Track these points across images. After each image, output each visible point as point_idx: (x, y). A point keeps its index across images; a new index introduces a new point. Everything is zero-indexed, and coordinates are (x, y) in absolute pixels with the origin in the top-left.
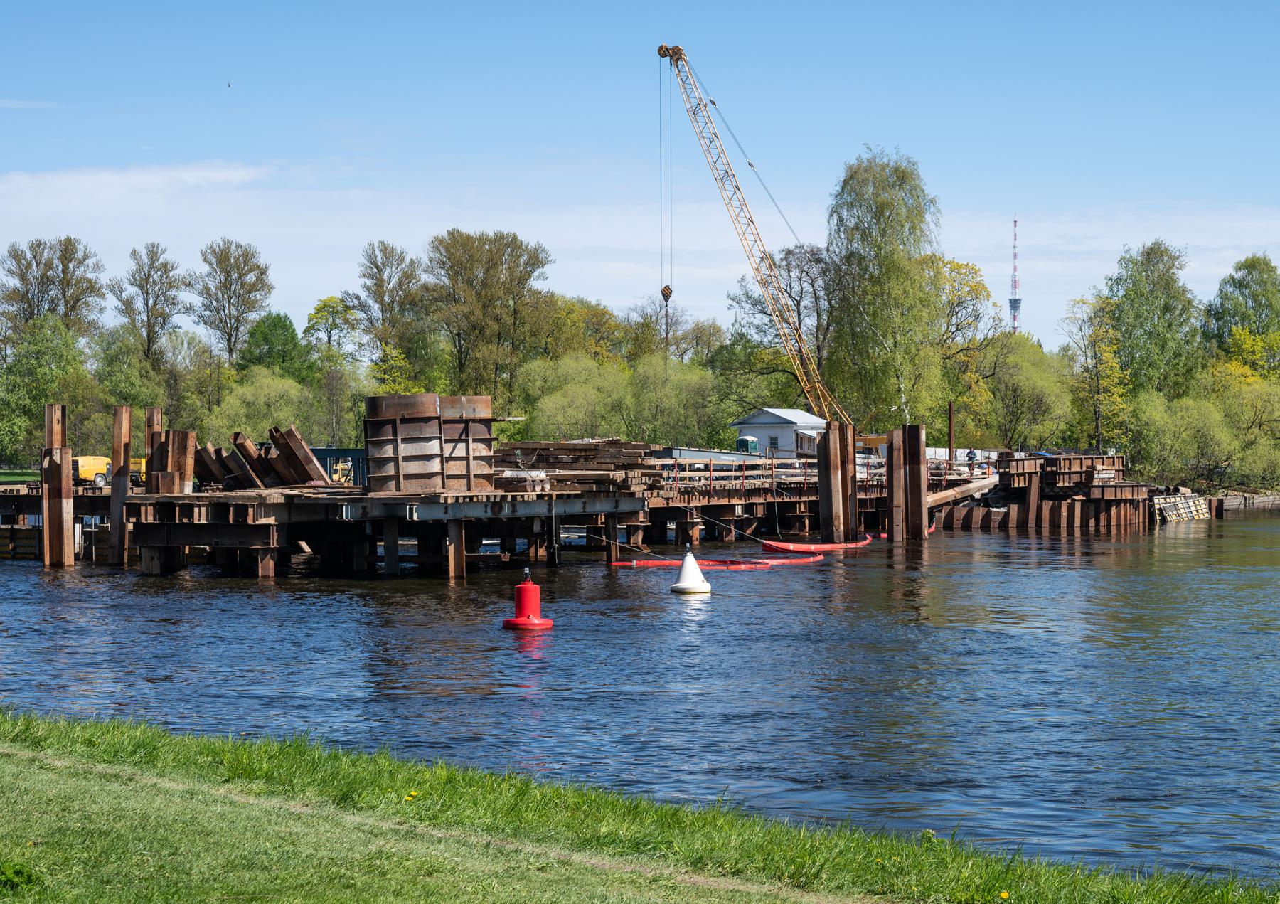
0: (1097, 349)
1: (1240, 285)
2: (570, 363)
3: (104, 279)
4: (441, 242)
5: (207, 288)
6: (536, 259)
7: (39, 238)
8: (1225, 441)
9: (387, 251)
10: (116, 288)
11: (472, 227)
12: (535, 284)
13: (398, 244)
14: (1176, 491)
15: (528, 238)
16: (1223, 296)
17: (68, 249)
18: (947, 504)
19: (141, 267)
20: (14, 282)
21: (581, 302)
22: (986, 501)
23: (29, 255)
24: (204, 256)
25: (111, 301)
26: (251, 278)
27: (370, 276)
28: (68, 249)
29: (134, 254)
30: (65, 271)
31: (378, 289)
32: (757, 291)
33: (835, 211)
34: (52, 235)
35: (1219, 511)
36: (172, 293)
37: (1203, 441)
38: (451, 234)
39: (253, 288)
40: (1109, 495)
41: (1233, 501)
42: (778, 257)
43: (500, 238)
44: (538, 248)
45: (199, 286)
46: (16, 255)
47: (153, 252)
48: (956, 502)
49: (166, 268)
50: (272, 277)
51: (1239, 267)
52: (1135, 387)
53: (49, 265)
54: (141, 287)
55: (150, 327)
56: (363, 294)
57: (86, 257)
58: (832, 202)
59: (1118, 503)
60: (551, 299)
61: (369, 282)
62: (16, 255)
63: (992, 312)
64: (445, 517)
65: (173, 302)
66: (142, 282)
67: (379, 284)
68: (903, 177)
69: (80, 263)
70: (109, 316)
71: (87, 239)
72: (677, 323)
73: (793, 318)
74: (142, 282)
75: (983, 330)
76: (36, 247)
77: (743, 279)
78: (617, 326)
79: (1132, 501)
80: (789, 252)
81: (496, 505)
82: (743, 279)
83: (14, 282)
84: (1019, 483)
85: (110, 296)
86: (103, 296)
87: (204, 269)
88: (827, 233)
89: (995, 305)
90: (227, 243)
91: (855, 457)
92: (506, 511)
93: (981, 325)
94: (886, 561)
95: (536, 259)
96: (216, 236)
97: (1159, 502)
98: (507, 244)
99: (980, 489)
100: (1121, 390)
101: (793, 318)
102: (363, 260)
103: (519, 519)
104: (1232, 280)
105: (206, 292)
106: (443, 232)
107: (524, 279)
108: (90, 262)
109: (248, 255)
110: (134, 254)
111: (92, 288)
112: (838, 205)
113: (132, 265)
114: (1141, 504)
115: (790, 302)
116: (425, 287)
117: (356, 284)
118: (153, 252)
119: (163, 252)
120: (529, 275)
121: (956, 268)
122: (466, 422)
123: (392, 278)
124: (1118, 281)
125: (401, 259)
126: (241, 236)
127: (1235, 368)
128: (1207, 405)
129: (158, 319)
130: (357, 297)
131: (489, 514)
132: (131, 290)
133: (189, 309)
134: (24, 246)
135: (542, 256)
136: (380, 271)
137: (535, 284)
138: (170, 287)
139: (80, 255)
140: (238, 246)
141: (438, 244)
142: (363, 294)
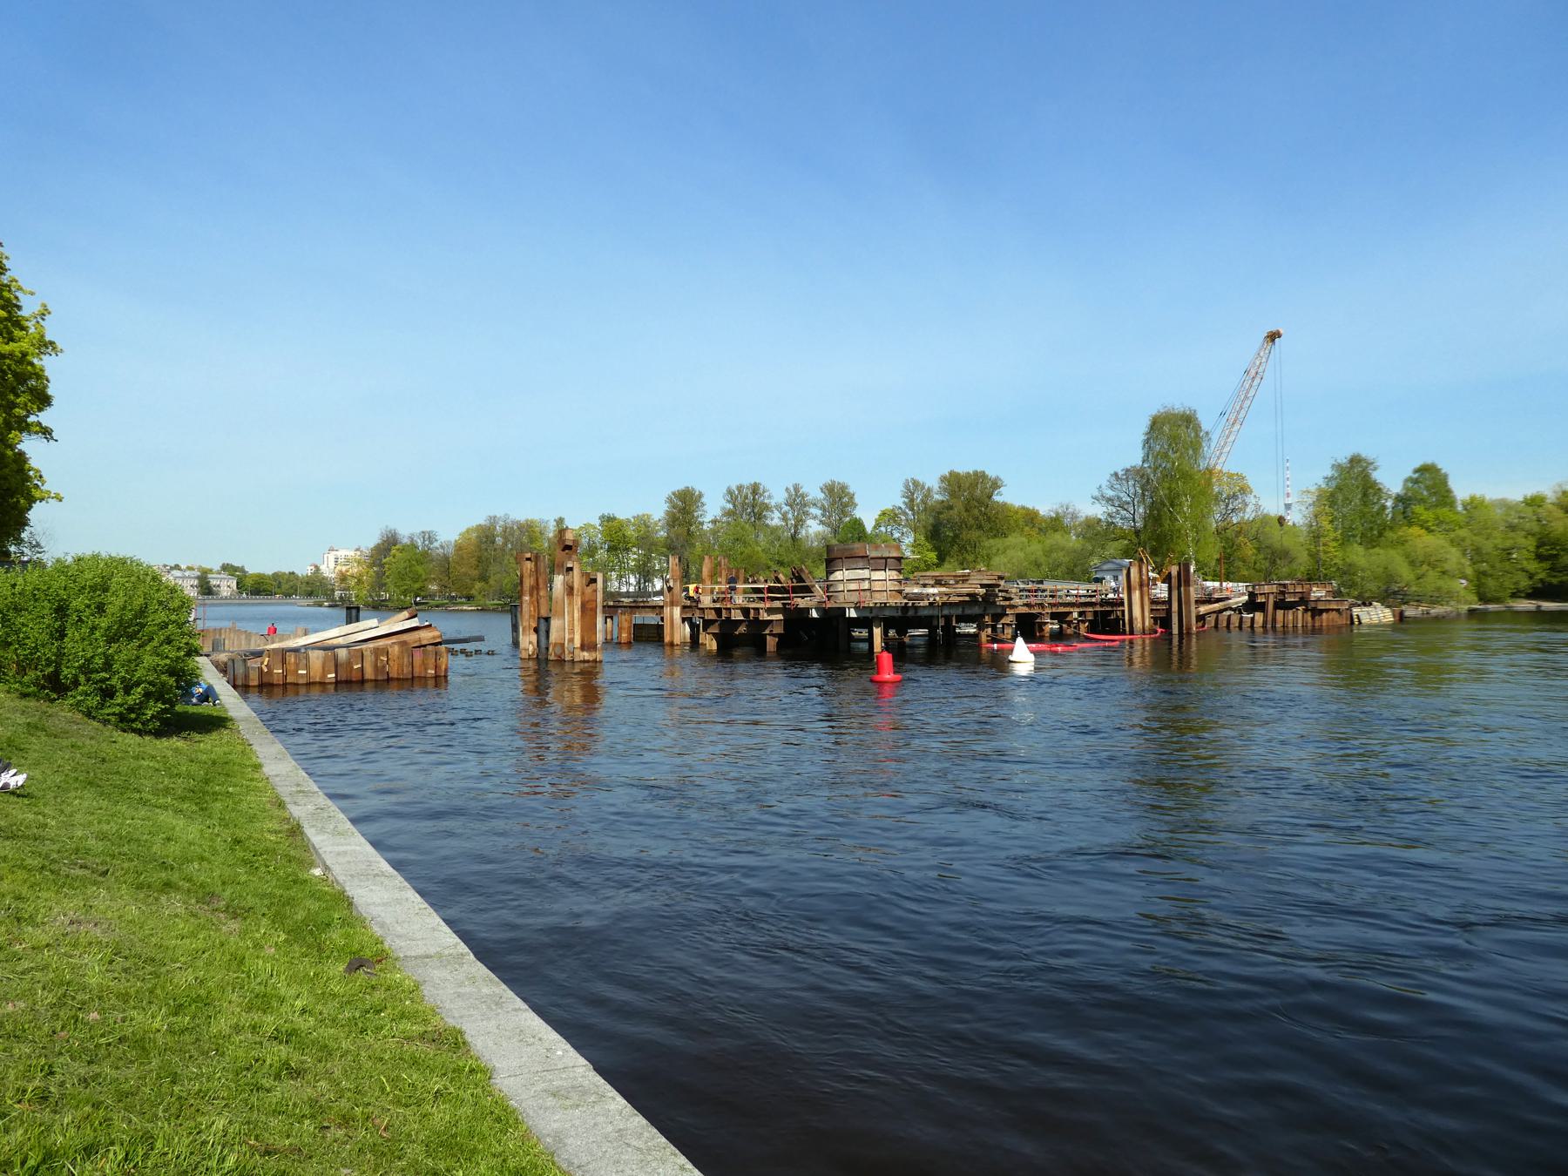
1: (1416, 481)
2: (1013, 539)
5: (823, 505)
6: (996, 484)
8: (1405, 573)
9: (916, 483)
10: (779, 507)
12: (996, 498)
13: (921, 479)
14: (1370, 604)
15: (991, 473)
16: (1405, 488)
17: (755, 489)
18: (1214, 612)
19: (790, 495)
20: (730, 506)
21: (1023, 508)
22: (1238, 610)
25: (777, 515)
26: (846, 499)
27: (907, 497)
28: (755, 489)
29: (787, 489)
30: (754, 499)
31: (911, 503)
32: (1110, 493)
33: (1147, 441)
34: (747, 481)
35: (1401, 617)
36: (807, 509)
37: (1390, 578)
38: (951, 473)
39: (847, 505)
40: (1321, 606)
41: (1410, 612)
42: (1120, 473)
43: (976, 473)
44: (998, 478)
45: (819, 505)
46: (730, 492)
47: (796, 488)
48: (1221, 611)
49: (803, 496)
50: (857, 499)
51: (1416, 471)
52: (1345, 541)
53: (746, 497)
54: (791, 506)
55: (796, 526)
56: (903, 507)
57: (764, 492)
58: (1144, 437)
59: (1327, 611)
61: (906, 500)
63: (1254, 501)
64: (870, 616)
65: (806, 513)
67: (912, 500)
68: (1188, 420)
69: (761, 495)
70: (775, 520)
72: (1076, 517)
73: (1131, 509)
75: (1249, 514)
76: (740, 488)
78: (1017, 512)
79: (1338, 610)
80: (1127, 470)
81: (905, 608)
83: (730, 506)
84: (1260, 600)
86: (772, 511)
87: (822, 496)
89: (1255, 496)
91: (1170, 594)
92: (911, 613)
93: (1248, 510)
94: (1167, 647)
95: (996, 484)
96: (827, 480)
97: (1356, 611)
98: (980, 477)
99: (1236, 603)
100: (1335, 544)
101: (1131, 509)
103: (920, 617)
104: (1409, 480)
105: (823, 508)
107: (990, 497)
108: (767, 494)
109: (843, 488)
110: (787, 489)
111: (767, 507)
112: (1148, 439)
115: (1129, 499)
116: (937, 501)
117: (900, 502)
118: (796, 488)
121: (1230, 476)
122: (886, 558)
123: (918, 497)
124: (1332, 478)
125: (923, 487)
126: (840, 478)
127: (1415, 530)
128: (1392, 552)
129: (799, 522)
130: (900, 508)
131: (900, 614)
132: (786, 508)
133: (815, 518)
134: (734, 488)
135: (999, 483)
136: (913, 494)
137: (996, 498)
138: (805, 505)
139: (761, 491)
140: (839, 483)
141: (943, 479)
142: (903, 507)
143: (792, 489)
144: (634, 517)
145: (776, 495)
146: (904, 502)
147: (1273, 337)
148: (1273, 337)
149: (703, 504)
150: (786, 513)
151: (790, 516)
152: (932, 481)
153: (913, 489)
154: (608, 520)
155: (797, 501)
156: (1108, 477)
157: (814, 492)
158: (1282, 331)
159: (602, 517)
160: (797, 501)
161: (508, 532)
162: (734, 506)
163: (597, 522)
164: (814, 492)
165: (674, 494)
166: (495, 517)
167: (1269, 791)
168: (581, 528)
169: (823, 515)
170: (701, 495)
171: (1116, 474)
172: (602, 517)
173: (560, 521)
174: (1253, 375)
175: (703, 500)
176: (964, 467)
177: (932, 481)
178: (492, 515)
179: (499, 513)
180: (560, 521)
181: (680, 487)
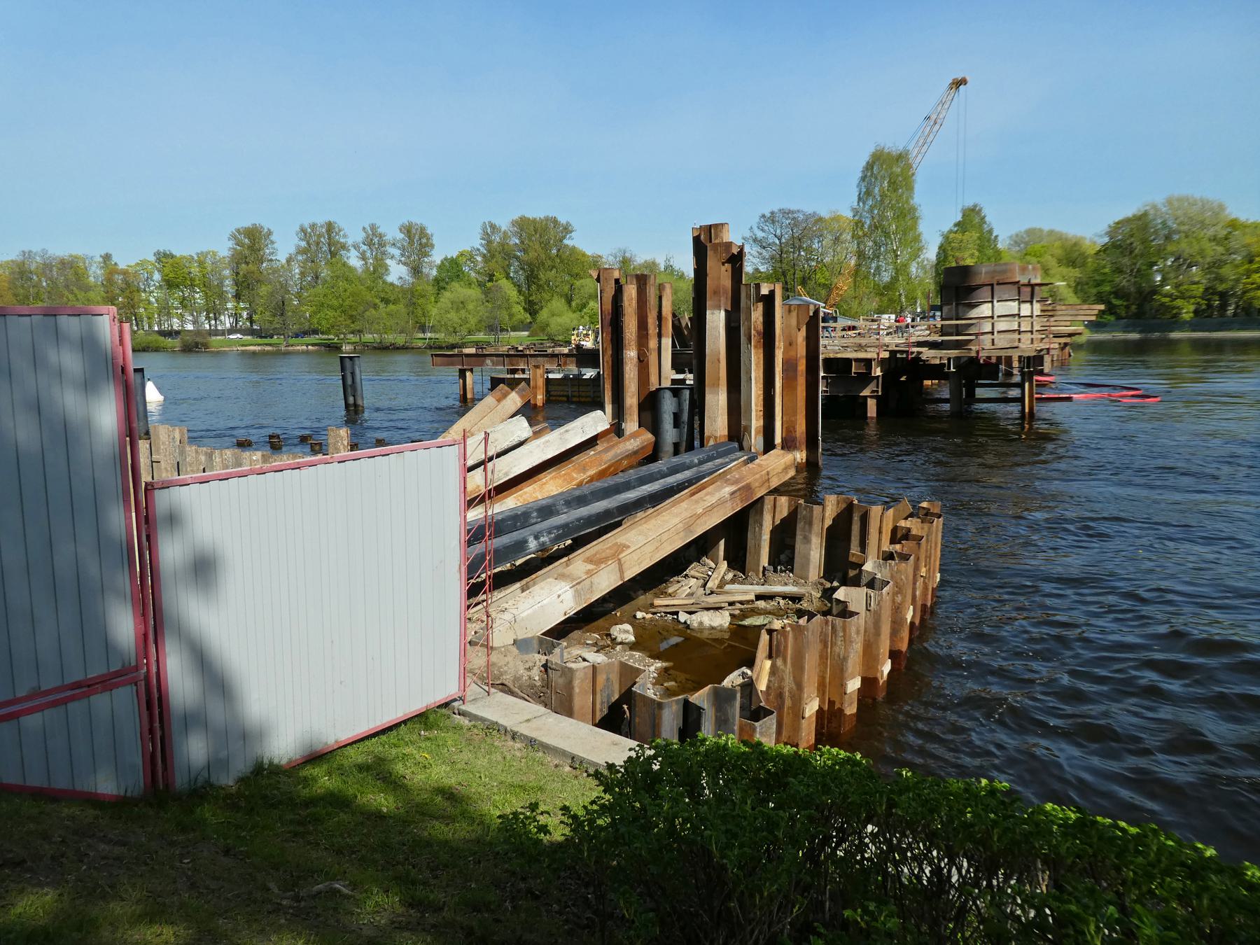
0: (574, 399)
3: (350, 241)
4: (516, 222)
6: (567, 229)
7: (253, 222)
9: (493, 226)
11: (531, 214)
12: (566, 242)
13: (497, 222)
15: (563, 219)
17: (330, 227)
20: (303, 244)
23: (309, 230)
24: (401, 230)
27: (483, 239)
28: (330, 227)
29: (364, 228)
34: (321, 220)
39: (426, 245)
46: (303, 230)
49: (381, 236)
50: (435, 241)
51: (956, 225)
57: (340, 231)
60: (573, 250)
61: (483, 242)
62: (303, 230)
65: (384, 253)
66: (370, 243)
68: (111, 255)
71: (341, 222)
74: (370, 243)
76: (313, 226)
77: (751, 228)
82: (751, 228)
83: (303, 244)
85: (352, 250)
88: (857, 194)
90: (28, 255)
95: (567, 229)
96: (404, 220)
102: (481, 231)
105: (403, 249)
106: (516, 217)
108: (342, 233)
109: (422, 231)
111: (344, 247)
113: (364, 235)
114: (778, 440)
118: (373, 227)
119: (379, 227)
120: (564, 237)
123: (497, 238)
126: (417, 220)
130: (478, 250)
132: (365, 248)
133: (392, 257)
134: (306, 225)
137: (566, 242)
141: (514, 223)
143: (369, 229)
144: (198, 254)
145: (353, 234)
146: (481, 244)
147: (959, 83)
148: (959, 83)
149: (273, 243)
150: (364, 251)
151: (368, 254)
152: (504, 223)
153: (489, 230)
154: (164, 258)
155: (374, 240)
156: (757, 219)
157: (392, 232)
158: (968, 79)
159: (158, 254)
160: (374, 240)
161: (47, 266)
162: (308, 243)
163: (153, 259)
164: (392, 232)
165: (238, 231)
166: (30, 252)
167: (1091, 524)
168: (137, 264)
169: (402, 255)
170: (270, 233)
171: (763, 216)
172: (158, 254)
173: (107, 257)
174: (932, 121)
175: (273, 238)
176: (537, 212)
177: (504, 223)
178: (26, 250)
179: (36, 248)
180: (107, 257)
181: (247, 223)
